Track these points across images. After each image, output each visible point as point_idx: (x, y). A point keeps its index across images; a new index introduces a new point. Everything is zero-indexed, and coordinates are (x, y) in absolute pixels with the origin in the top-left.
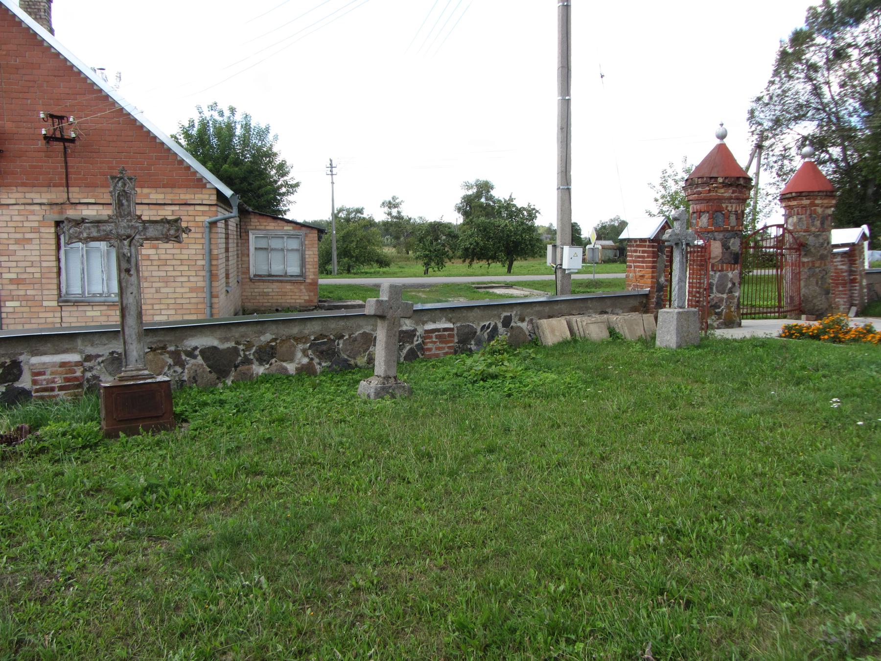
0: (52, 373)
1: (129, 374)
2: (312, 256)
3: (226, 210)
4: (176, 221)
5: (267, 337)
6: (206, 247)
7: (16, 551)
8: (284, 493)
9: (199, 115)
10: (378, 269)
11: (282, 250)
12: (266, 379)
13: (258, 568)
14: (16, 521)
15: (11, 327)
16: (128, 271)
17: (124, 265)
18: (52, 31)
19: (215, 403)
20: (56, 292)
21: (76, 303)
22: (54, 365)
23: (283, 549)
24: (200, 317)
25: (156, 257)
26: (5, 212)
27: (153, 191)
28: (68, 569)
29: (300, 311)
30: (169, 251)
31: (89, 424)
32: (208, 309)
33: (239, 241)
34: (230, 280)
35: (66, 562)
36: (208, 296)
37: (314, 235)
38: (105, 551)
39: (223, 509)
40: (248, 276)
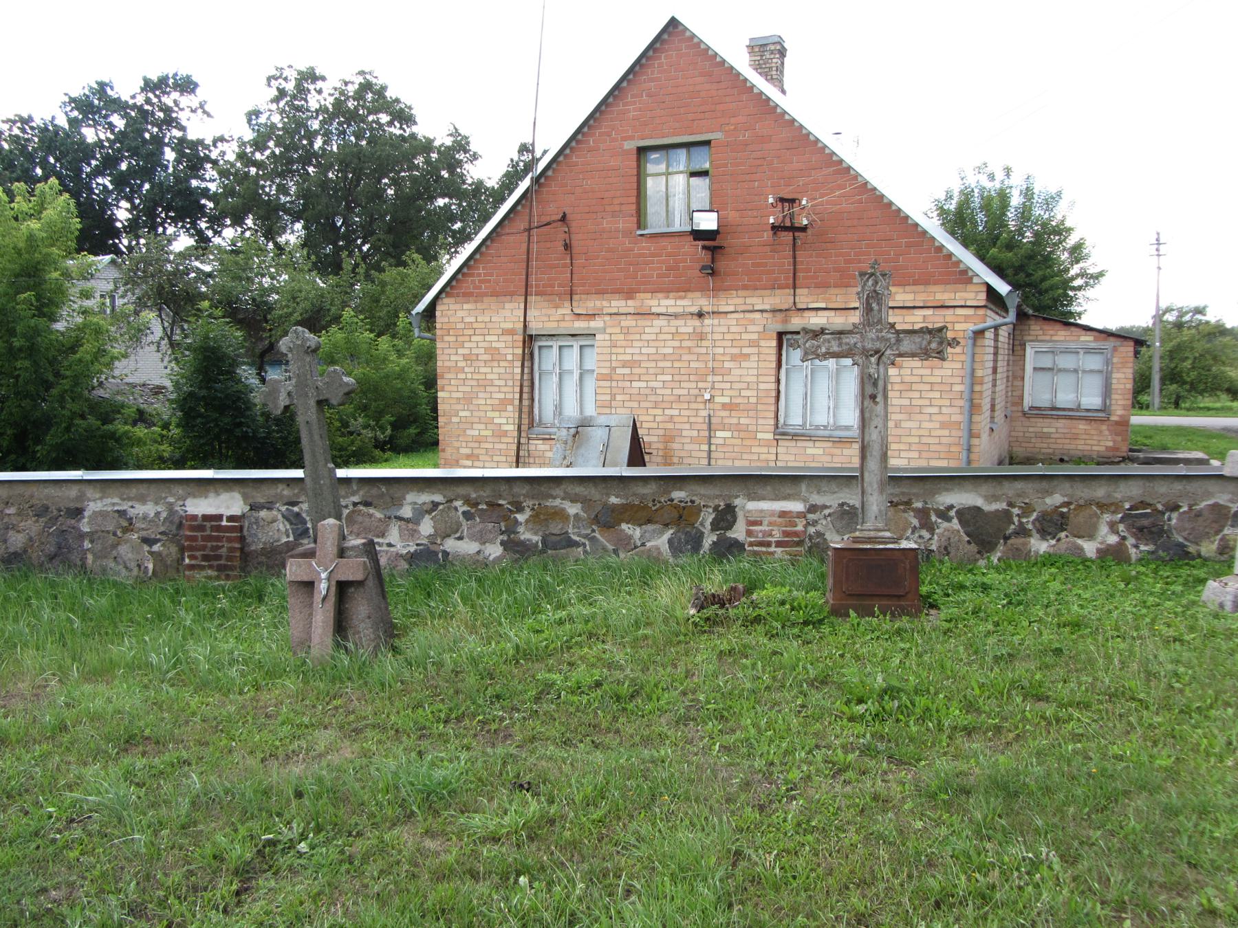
0: (770, 524)
1: (866, 534)
2: (1124, 381)
3: (997, 313)
4: (940, 330)
5: (1056, 499)
6: (968, 365)
7: (730, 739)
8: (1082, 735)
9: (961, 182)
10: (1229, 404)
11: (1076, 371)
12: (1049, 560)
13: (1046, 837)
14: (729, 703)
15: (720, 462)
16: (873, 397)
17: (869, 390)
18: (783, 92)
19: (975, 587)
20: (772, 422)
21: (795, 437)
22: (772, 513)
23: (1082, 819)
24: (953, 464)
25: (898, 380)
26: (723, 321)
27: (900, 289)
28: (790, 776)
29: (1098, 464)
30: (915, 372)
31: (812, 594)
32: (965, 453)
33: (1011, 358)
34: (996, 414)
35: (787, 767)
36: (966, 435)
37: (1128, 349)
38: (834, 764)
39: (990, 740)
40: (1020, 409)
